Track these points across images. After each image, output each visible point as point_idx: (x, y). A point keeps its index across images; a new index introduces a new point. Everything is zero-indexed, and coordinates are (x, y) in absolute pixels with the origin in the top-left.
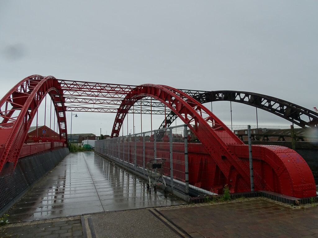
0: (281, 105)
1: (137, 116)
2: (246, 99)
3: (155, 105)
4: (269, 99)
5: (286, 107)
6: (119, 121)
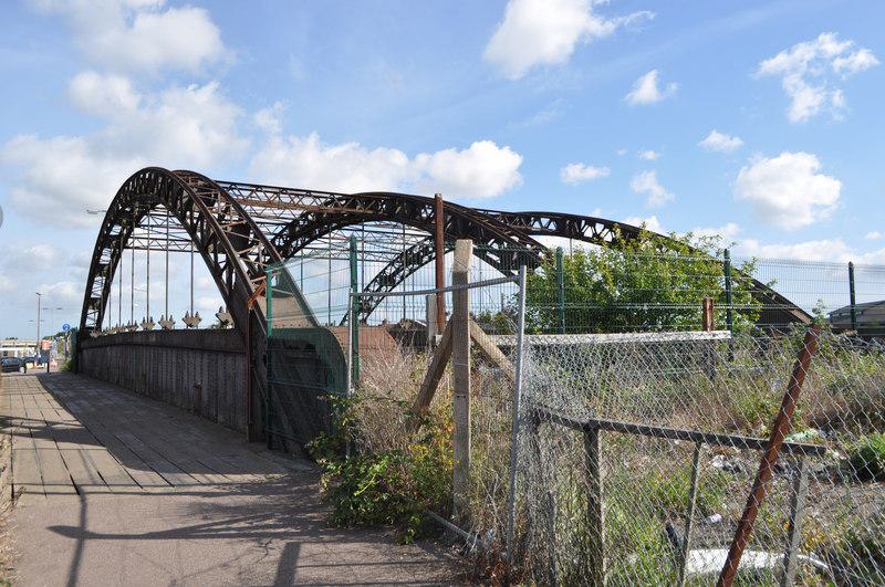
5: (654, 218)
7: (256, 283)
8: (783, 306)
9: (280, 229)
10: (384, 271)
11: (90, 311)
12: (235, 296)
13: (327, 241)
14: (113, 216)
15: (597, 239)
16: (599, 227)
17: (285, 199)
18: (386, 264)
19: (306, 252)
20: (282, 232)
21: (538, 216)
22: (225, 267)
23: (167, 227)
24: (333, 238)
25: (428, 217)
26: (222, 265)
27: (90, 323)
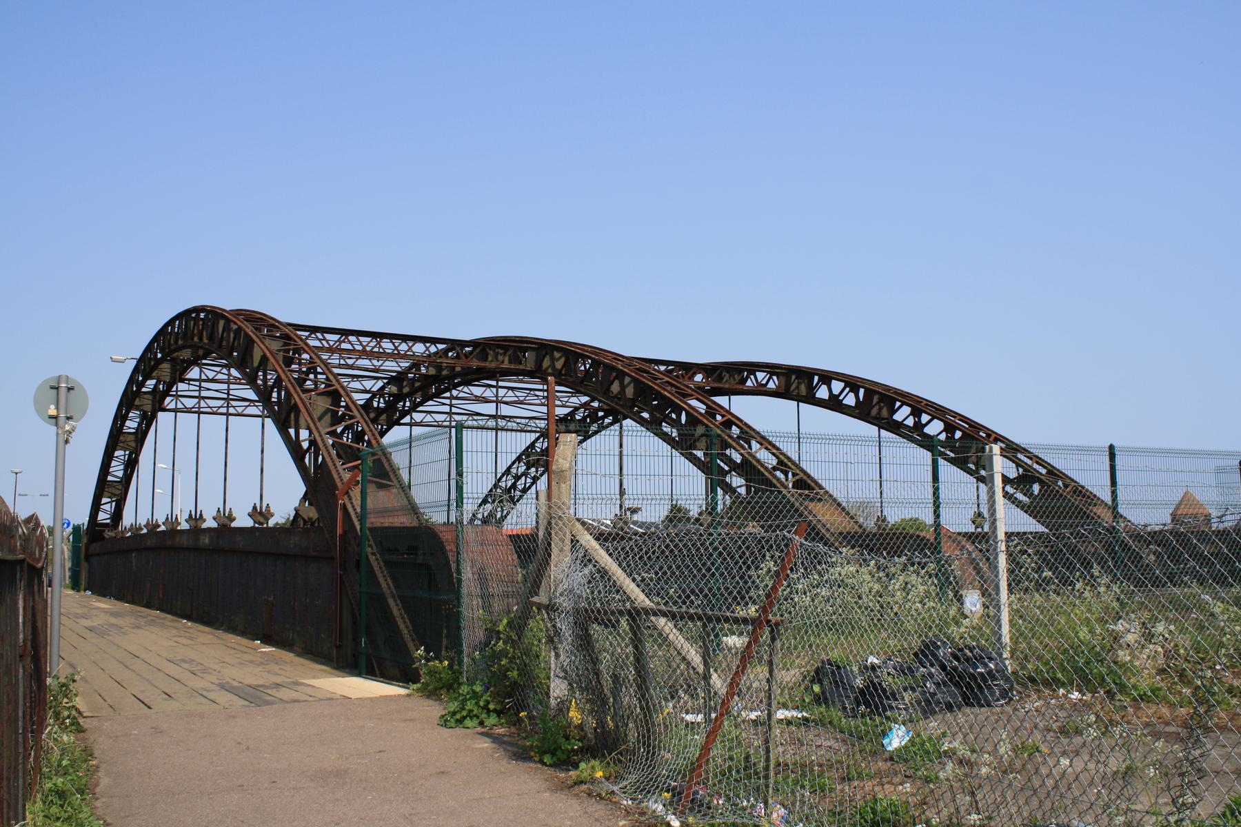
0: (949, 428)
1: (213, 425)
2: (850, 400)
3: (510, 397)
4: (919, 406)
5: (818, 395)
6: (125, 442)
7: (350, 469)
8: (1077, 501)
9: (380, 384)
10: (532, 445)
11: (104, 500)
12: (319, 485)
13: (448, 402)
14: (145, 366)
15: (834, 404)
16: (837, 386)
17: (387, 345)
18: (534, 436)
19: (417, 417)
20: (382, 388)
21: (753, 367)
22: (309, 448)
23: (228, 383)
24: (457, 398)
25: (587, 371)
26: (305, 445)
27: (103, 517)
